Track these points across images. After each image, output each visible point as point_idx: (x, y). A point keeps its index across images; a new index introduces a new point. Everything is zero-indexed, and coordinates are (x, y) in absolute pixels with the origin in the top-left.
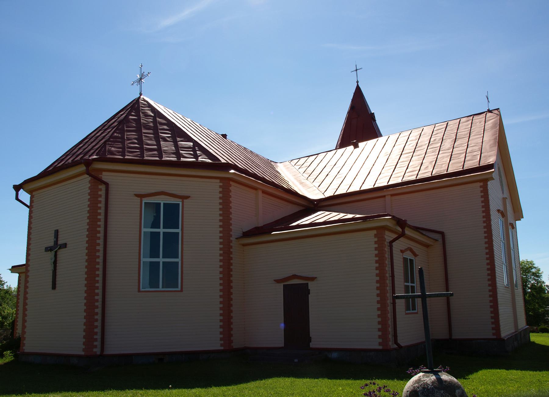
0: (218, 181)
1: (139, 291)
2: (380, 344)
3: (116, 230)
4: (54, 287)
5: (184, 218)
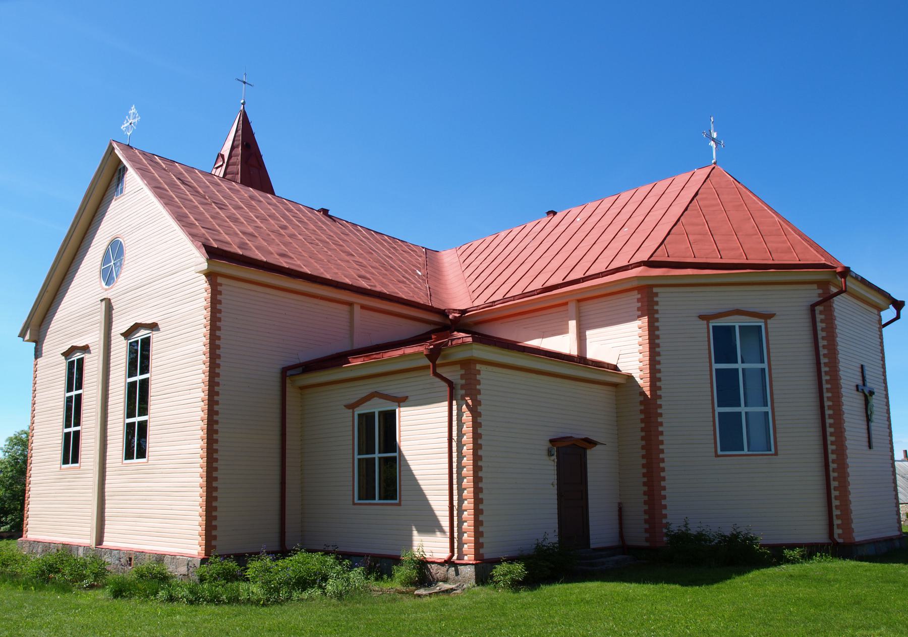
0: (815, 286)
1: (717, 456)
2: (647, 540)
3: (249, 386)
4: (870, 446)
5: (771, 342)
